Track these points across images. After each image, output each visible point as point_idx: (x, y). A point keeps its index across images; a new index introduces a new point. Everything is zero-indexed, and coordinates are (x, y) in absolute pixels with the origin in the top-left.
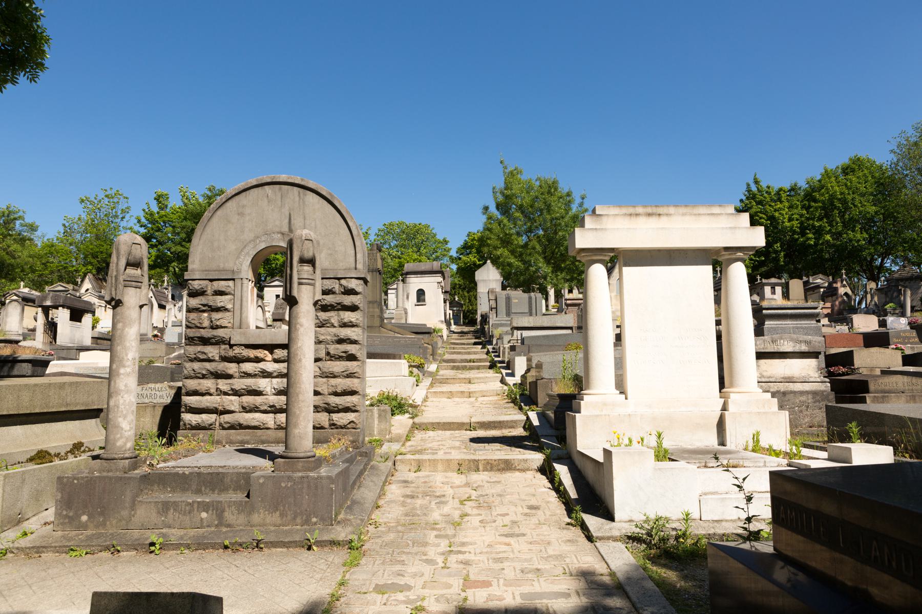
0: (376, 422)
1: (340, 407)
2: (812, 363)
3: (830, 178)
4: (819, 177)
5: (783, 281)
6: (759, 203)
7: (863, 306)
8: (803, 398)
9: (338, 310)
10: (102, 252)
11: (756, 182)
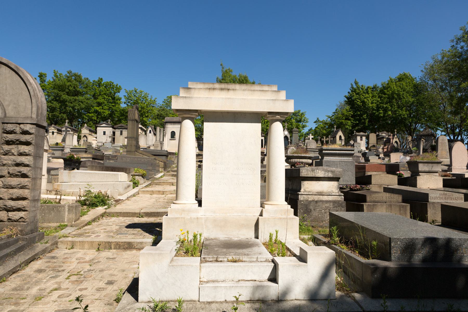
0: (66, 213)
1: (14, 208)
6: (357, 94)
8: (327, 205)
9: (17, 144)
11: (356, 83)
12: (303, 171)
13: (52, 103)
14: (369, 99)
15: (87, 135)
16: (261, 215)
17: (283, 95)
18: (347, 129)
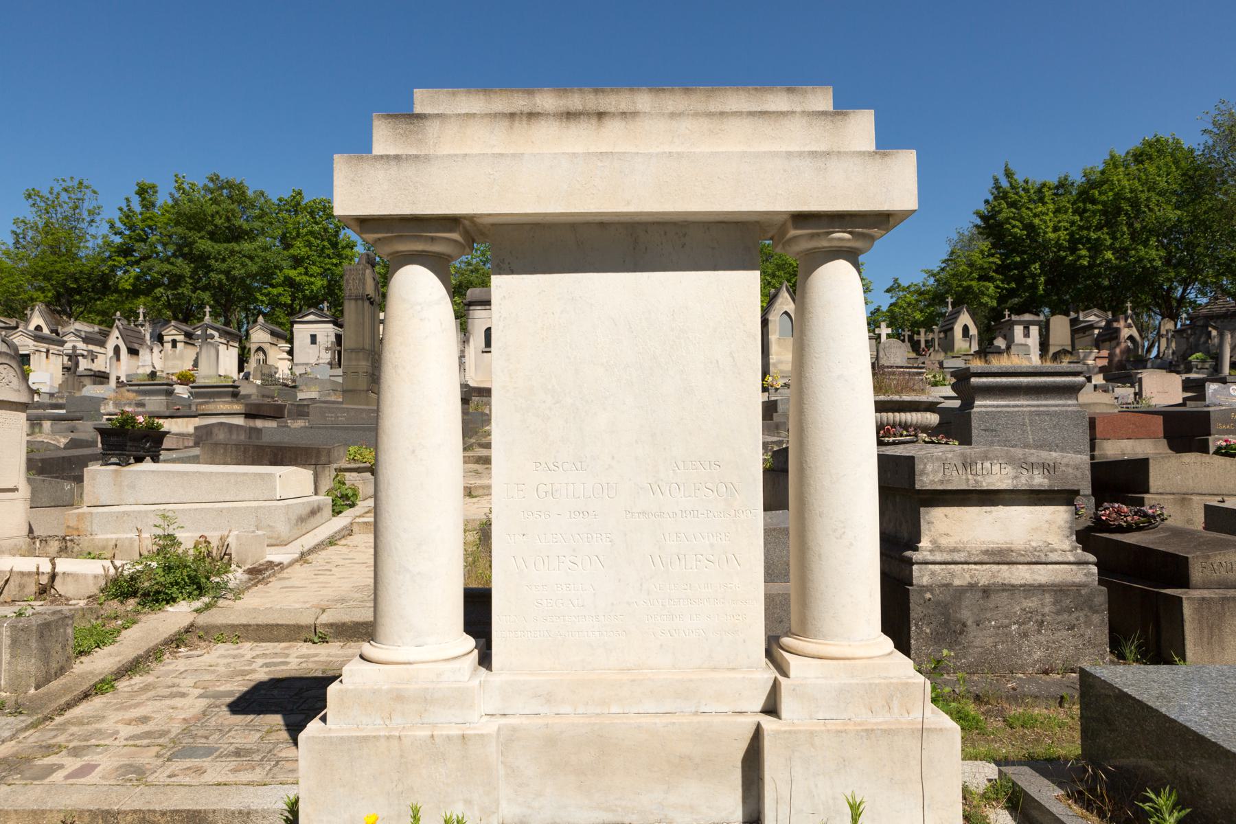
2: (1058, 515)
3: (1116, 167)
4: (1101, 167)
5: (1042, 317)
6: (1013, 205)
7: (1154, 353)
8: (1031, 603)
10: (58, 272)
11: (1009, 174)
12: (929, 468)
13: (172, 264)
14: (1047, 218)
15: (265, 346)
16: (771, 709)
17: (861, 128)
18: (985, 305)
